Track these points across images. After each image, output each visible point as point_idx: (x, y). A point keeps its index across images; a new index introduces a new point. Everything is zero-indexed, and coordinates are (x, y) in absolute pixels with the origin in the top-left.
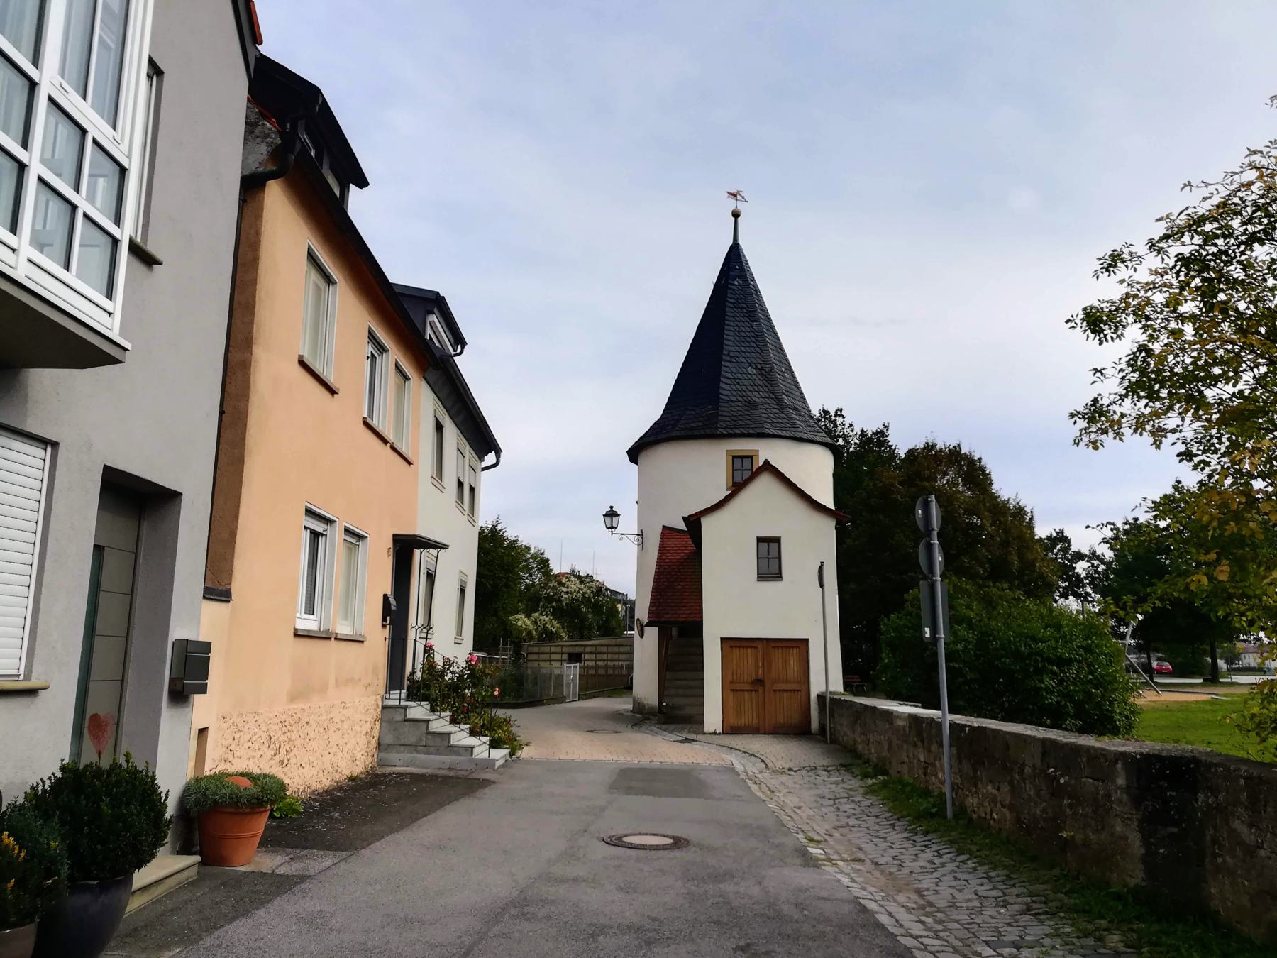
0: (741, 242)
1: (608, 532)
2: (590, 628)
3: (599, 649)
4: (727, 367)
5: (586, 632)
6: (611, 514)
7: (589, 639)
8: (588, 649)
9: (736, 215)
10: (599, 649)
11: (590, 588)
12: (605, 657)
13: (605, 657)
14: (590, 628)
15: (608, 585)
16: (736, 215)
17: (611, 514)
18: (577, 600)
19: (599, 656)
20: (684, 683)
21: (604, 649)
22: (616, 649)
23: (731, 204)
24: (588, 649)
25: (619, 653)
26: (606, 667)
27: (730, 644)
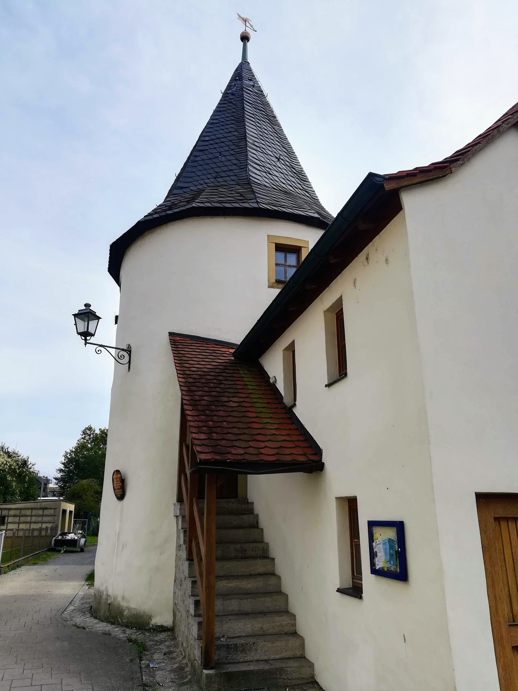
0: (250, 59)
1: (80, 340)
2: (13, 494)
3: (23, 512)
4: (252, 154)
5: (9, 498)
6: (87, 315)
7: (11, 502)
8: (12, 513)
9: (245, 38)
10: (23, 512)
11: (16, 461)
12: (28, 519)
13: (28, 519)
14: (13, 494)
15: (288, 139)
16: (245, 38)
17: (87, 315)
18: (4, 471)
19: (23, 519)
20: (232, 584)
21: (28, 512)
22: (40, 512)
23: (241, 29)
24: (12, 513)
25: (43, 516)
26: (40, 529)
27: (372, 524)
